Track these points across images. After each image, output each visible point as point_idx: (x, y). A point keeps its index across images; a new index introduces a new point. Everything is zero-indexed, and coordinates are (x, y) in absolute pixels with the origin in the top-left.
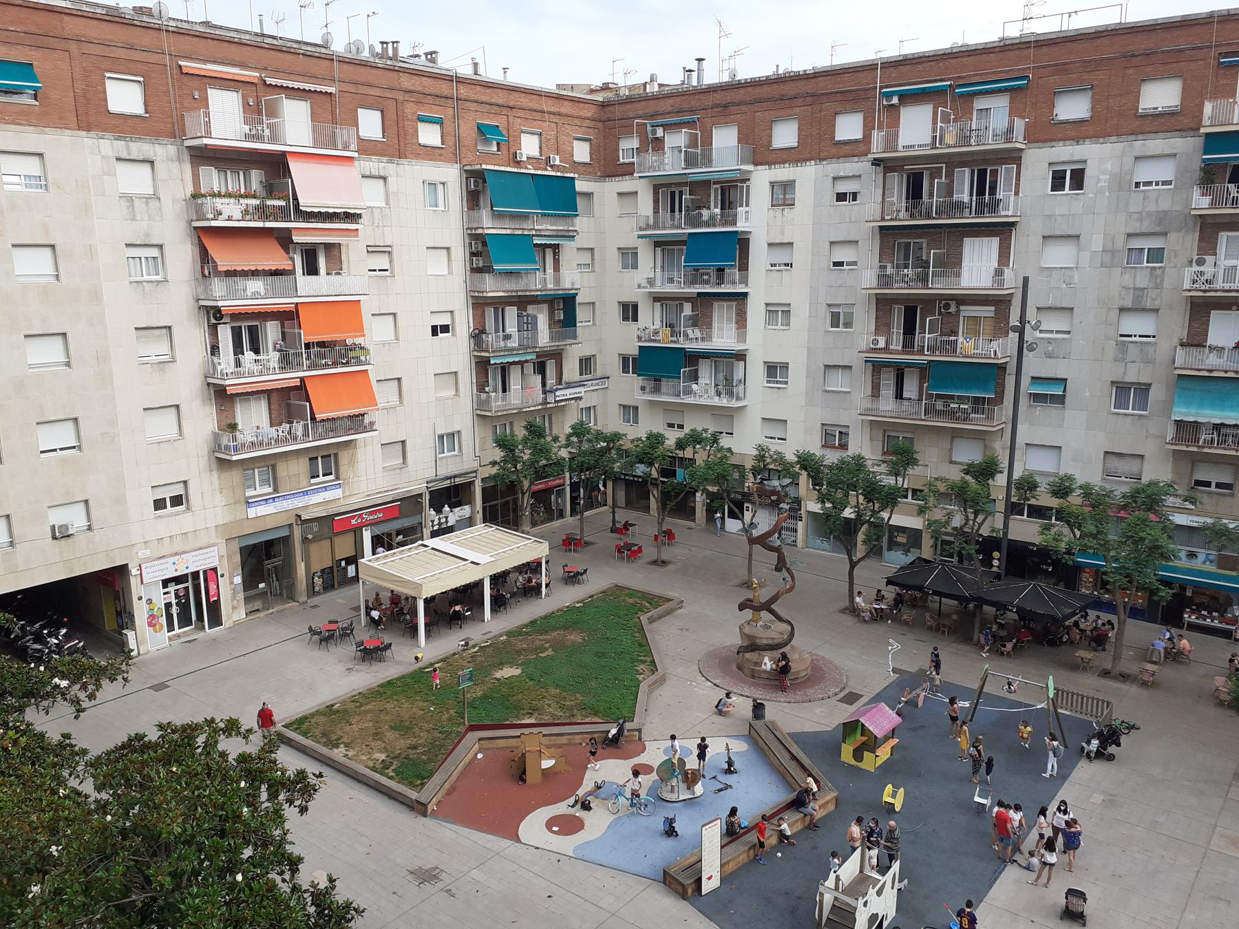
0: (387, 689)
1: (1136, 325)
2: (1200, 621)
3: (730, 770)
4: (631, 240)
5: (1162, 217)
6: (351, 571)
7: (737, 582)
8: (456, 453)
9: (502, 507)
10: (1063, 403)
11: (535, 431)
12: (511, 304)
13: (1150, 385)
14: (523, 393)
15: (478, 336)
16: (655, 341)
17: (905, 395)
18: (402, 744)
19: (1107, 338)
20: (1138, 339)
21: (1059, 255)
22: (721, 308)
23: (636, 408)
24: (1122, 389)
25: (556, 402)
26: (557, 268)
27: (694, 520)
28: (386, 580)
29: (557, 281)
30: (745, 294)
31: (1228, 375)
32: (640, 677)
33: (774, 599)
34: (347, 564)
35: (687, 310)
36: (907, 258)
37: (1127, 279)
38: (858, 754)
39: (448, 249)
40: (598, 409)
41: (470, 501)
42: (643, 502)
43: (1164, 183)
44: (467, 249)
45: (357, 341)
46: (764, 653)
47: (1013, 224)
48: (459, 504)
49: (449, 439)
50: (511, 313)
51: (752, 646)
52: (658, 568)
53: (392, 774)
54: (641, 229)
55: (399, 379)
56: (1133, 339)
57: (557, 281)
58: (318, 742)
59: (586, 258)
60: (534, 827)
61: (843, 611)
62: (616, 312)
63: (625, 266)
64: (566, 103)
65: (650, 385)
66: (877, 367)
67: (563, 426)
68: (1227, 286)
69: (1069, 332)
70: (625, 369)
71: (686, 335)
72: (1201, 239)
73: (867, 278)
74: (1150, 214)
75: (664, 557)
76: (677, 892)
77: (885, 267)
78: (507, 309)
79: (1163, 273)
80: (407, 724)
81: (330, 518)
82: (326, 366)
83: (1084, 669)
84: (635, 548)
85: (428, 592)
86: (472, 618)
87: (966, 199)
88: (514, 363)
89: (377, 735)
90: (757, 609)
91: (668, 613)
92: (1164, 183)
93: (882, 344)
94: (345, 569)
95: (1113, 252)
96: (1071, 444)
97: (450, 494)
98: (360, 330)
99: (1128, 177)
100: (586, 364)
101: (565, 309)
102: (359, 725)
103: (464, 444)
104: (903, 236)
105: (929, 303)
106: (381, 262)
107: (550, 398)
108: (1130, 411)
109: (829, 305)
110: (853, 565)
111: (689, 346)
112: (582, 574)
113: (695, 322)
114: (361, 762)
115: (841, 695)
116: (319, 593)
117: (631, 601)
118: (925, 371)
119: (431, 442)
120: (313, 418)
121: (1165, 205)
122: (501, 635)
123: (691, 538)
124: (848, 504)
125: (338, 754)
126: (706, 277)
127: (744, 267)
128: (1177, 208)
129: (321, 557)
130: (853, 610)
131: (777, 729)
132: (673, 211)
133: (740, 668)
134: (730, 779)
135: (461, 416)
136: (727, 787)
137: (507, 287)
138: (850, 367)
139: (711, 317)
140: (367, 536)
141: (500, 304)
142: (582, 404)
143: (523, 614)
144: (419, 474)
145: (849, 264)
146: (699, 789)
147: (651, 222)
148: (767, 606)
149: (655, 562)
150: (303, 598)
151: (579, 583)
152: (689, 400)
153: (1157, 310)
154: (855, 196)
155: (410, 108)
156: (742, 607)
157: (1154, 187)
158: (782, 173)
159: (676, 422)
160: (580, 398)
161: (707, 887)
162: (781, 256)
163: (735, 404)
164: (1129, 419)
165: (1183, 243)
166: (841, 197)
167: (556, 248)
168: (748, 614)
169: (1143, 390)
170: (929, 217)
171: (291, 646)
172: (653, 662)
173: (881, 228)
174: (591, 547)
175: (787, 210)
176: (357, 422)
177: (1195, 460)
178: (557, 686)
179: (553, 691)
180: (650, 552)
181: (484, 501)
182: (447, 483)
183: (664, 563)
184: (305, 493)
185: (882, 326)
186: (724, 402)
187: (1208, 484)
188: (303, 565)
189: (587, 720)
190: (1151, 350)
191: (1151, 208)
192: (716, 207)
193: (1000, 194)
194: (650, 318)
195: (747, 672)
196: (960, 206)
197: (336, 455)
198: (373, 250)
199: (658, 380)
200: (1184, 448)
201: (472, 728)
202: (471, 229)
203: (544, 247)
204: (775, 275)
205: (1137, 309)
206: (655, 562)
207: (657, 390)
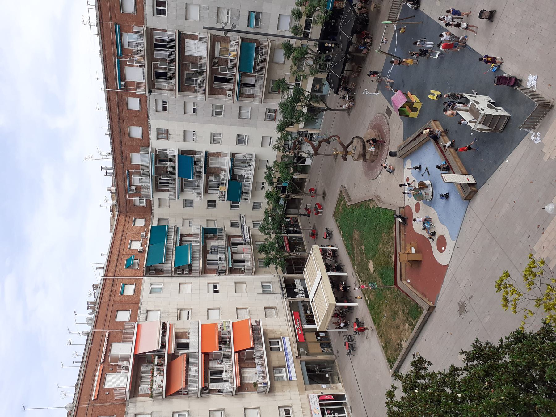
0: (376, 321)
4: (180, 202)
7: (334, 161)
8: (271, 285)
9: (296, 265)
12: (206, 257)
14: (245, 253)
15: (219, 272)
16: (225, 193)
23: (254, 203)
26: (191, 236)
27: (306, 179)
29: (196, 236)
30: (206, 152)
33: (342, 145)
35: (212, 178)
36: (193, 80)
38: (414, 110)
41: (293, 279)
42: (296, 201)
45: (219, 326)
46: (367, 150)
47: (180, 33)
49: (265, 288)
50: (210, 257)
51: (363, 155)
54: (175, 197)
55: (237, 309)
57: (196, 236)
58: (399, 354)
59: (187, 223)
61: (349, 114)
62: (211, 210)
63: (191, 205)
64: (118, 228)
65: (244, 196)
66: (241, 95)
67: (261, 236)
69: (228, 10)
71: (223, 179)
73: (201, 98)
75: (321, 193)
76: (474, 194)
77: (196, 90)
78: (208, 258)
81: (298, 343)
82: (230, 341)
83: (379, 7)
84: (317, 206)
85: (333, 301)
86: (346, 281)
87: (168, 53)
88: (232, 257)
89: (397, 327)
90: (347, 153)
91: (347, 193)
93: (230, 93)
94: (321, 337)
97: (289, 288)
98: (215, 325)
100: (234, 224)
101: (209, 233)
102: (392, 335)
103: (267, 281)
104: (183, 82)
105: (213, 71)
106: (184, 314)
107: (248, 241)
109: (212, 115)
110: (328, 109)
111: (228, 178)
113: (217, 175)
114: (409, 335)
115: (387, 116)
116: (332, 350)
118: (243, 74)
119: (266, 296)
120: (253, 348)
122: (354, 268)
123: (313, 180)
124: (299, 110)
125: (405, 345)
126: (198, 170)
127: (194, 153)
129: (315, 348)
130: (349, 109)
131: (401, 146)
132: (168, 183)
133: (373, 161)
134: (424, 168)
135: (255, 282)
136: (427, 169)
137: (198, 258)
138: (240, 107)
140: (307, 327)
141: (206, 262)
142: (251, 227)
143: (344, 258)
144: (280, 302)
145: (194, 106)
147: (172, 193)
148: (346, 148)
149: (324, 198)
150: (334, 357)
151: (332, 232)
152: (252, 179)
154: (164, 102)
155: (117, 298)
156: (345, 159)
158: (153, 134)
159: (261, 185)
160: (249, 228)
161: (472, 181)
162: (190, 136)
163: (254, 159)
166: (165, 108)
168: (348, 157)
170: (175, 70)
171: (355, 363)
172: (369, 200)
173: (179, 91)
174: (316, 227)
175: (170, 133)
176: (255, 329)
178: (378, 244)
179: (380, 246)
180: (319, 200)
182: (284, 289)
184: (286, 354)
185: (222, 92)
186: (253, 163)
188: (318, 356)
189: (394, 231)
194: (215, 195)
196: (171, 56)
198: (179, 318)
199: (242, 193)
201: (396, 284)
203: (181, 241)
206: (324, 198)
207: (247, 193)
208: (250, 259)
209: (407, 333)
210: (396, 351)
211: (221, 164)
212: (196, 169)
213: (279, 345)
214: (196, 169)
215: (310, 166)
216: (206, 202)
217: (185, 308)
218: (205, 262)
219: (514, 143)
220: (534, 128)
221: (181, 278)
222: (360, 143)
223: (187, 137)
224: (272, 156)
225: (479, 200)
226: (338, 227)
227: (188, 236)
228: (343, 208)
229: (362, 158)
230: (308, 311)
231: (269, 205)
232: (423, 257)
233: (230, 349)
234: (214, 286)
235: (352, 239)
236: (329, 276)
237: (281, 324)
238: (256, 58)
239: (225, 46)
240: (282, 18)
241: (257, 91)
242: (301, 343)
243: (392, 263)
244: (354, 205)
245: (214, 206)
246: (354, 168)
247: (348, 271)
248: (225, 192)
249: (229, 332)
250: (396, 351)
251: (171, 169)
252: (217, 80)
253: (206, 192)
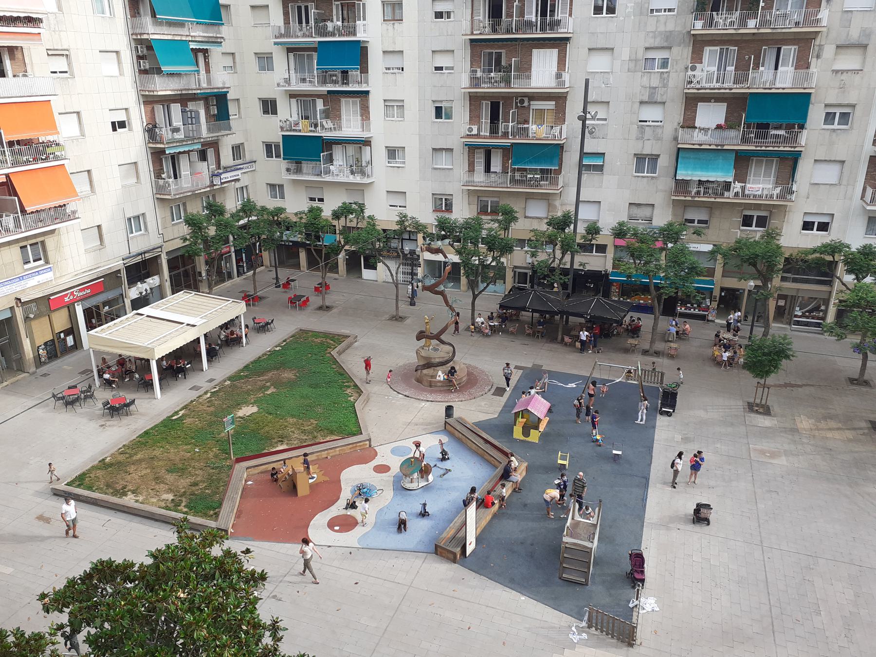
0: (146, 439)
1: (652, 114)
2: (687, 311)
3: (444, 457)
4: (267, 45)
5: (668, 35)
6: (70, 341)
7: (387, 317)
8: (143, 232)
9: (184, 274)
10: (602, 170)
11: (215, 210)
12: (175, 101)
13: (659, 156)
14: (193, 177)
15: (151, 131)
16: (295, 130)
18: (183, 483)
19: (632, 123)
20: (651, 124)
21: (599, 63)
22: (347, 103)
23: (281, 186)
24: (640, 159)
25: (222, 183)
26: (208, 71)
27: (337, 273)
28: (117, 347)
29: (209, 81)
30: (367, 92)
31: (703, 147)
32: (352, 399)
34: (66, 336)
35: (320, 105)
36: (490, 65)
37: (645, 81)
39: (117, 52)
41: (158, 272)
42: (292, 261)
43: (670, 10)
44: (134, 52)
45: (51, 138)
46: (438, 368)
47: (567, 39)
48: (148, 276)
49: (135, 222)
50: (176, 108)
51: (429, 365)
52: (325, 312)
53: (185, 510)
54: (276, 37)
55: (89, 171)
56: (648, 123)
57: (209, 81)
58: (106, 494)
59: (229, 61)
60: (318, 528)
62: (258, 108)
63: (262, 68)
65: (293, 166)
66: (472, 149)
67: (231, 204)
68: (707, 86)
69: (605, 120)
70: (269, 154)
71: (322, 126)
72: (693, 52)
73: (463, 80)
74: (661, 33)
76: (448, 558)
77: (476, 71)
78: (173, 106)
79: (668, 76)
80: (180, 466)
81: (47, 298)
82: (27, 162)
84: (305, 299)
85: (158, 355)
86: (193, 369)
87: (534, 20)
88: (184, 152)
89: (158, 479)
92: (670, 10)
93: (475, 132)
94: (65, 340)
95: (636, 60)
96: (610, 199)
97: (140, 269)
98: (53, 127)
99: (646, 5)
100: (237, 150)
101: (219, 105)
102: (135, 474)
103: (149, 224)
104: (488, 47)
105: (508, 98)
106: (60, 64)
107: (217, 181)
108: (645, 174)
109: (434, 101)
111: (325, 134)
112: (270, 324)
113: (327, 114)
114: (153, 504)
116: (45, 363)
118: (507, 151)
119: (122, 225)
120: (23, 211)
121: (670, 27)
122: (225, 381)
124: (467, 251)
125: (129, 500)
126: (334, 78)
127: (364, 70)
128: (678, 29)
129: (42, 332)
130: (478, 330)
131: (466, 422)
132: (300, 22)
134: (447, 465)
135: (144, 201)
136: (448, 471)
137: (177, 86)
138: (451, 150)
139: (339, 110)
140: (79, 310)
141: (166, 101)
142: (238, 185)
143: (234, 362)
144: (116, 255)
145: (447, 68)
146: (431, 477)
147: (283, 32)
149: (320, 308)
150: (33, 369)
151: (268, 330)
152: (328, 178)
153: (664, 103)
154: (449, 14)
156: (419, 338)
157: (663, 13)
159: (317, 197)
160: (238, 180)
161: (470, 549)
162: (394, 61)
163: (366, 180)
164: (645, 179)
165: (682, 54)
166: (439, 15)
167: (205, 52)
169: (654, 158)
170: (509, 31)
171: (39, 412)
172: (356, 386)
173: (472, 41)
174: (264, 301)
175: (397, 24)
176: (60, 213)
177: (686, 205)
178: (293, 416)
180: (315, 300)
181: (171, 269)
182: (139, 259)
183: (328, 308)
184: (21, 278)
185: (474, 117)
186: (358, 179)
187: (692, 221)
188: (28, 340)
189: (328, 439)
190: (659, 131)
191: (662, 28)
192: (338, 20)
193: (559, 16)
194: (288, 112)
196: (529, 25)
197: (43, 243)
198: (52, 53)
199: (299, 163)
200: (683, 198)
201: (238, 460)
202: (136, 34)
203: (195, 51)
204: (390, 77)
205: (650, 102)
206: (320, 308)
207: (299, 171)
208: (181, 188)
209: (154, 500)
210: (108, 486)
211: (349, 120)
212: (335, 75)
213: (34, 261)
214: (335, 75)
215: (360, 277)
216: (272, 96)
217: (74, 64)
218: (166, 101)
219: (555, 603)
220: (589, 627)
221: (128, 53)
222: (447, 357)
223: (391, 56)
225: (443, 569)
226: (284, 341)
227: (207, 64)
228: (322, 343)
229: (421, 363)
230: (107, 308)
231: (296, 214)
232: (305, 497)
233: (15, 164)
234: (124, 122)
235: (278, 369)
236: (198, 339)
237: (76, 259)
238: (534, 171)
239: (549, 118)
241: (479, 176)
242: (46, 304)
244: (335, 362)
245: (266, 112)
247: (211, 370)
248: (300, 131)
249: (46, 160)
250: (108, 486)
251: (330, 29)
252: (495, 108)
253: (292, 95)
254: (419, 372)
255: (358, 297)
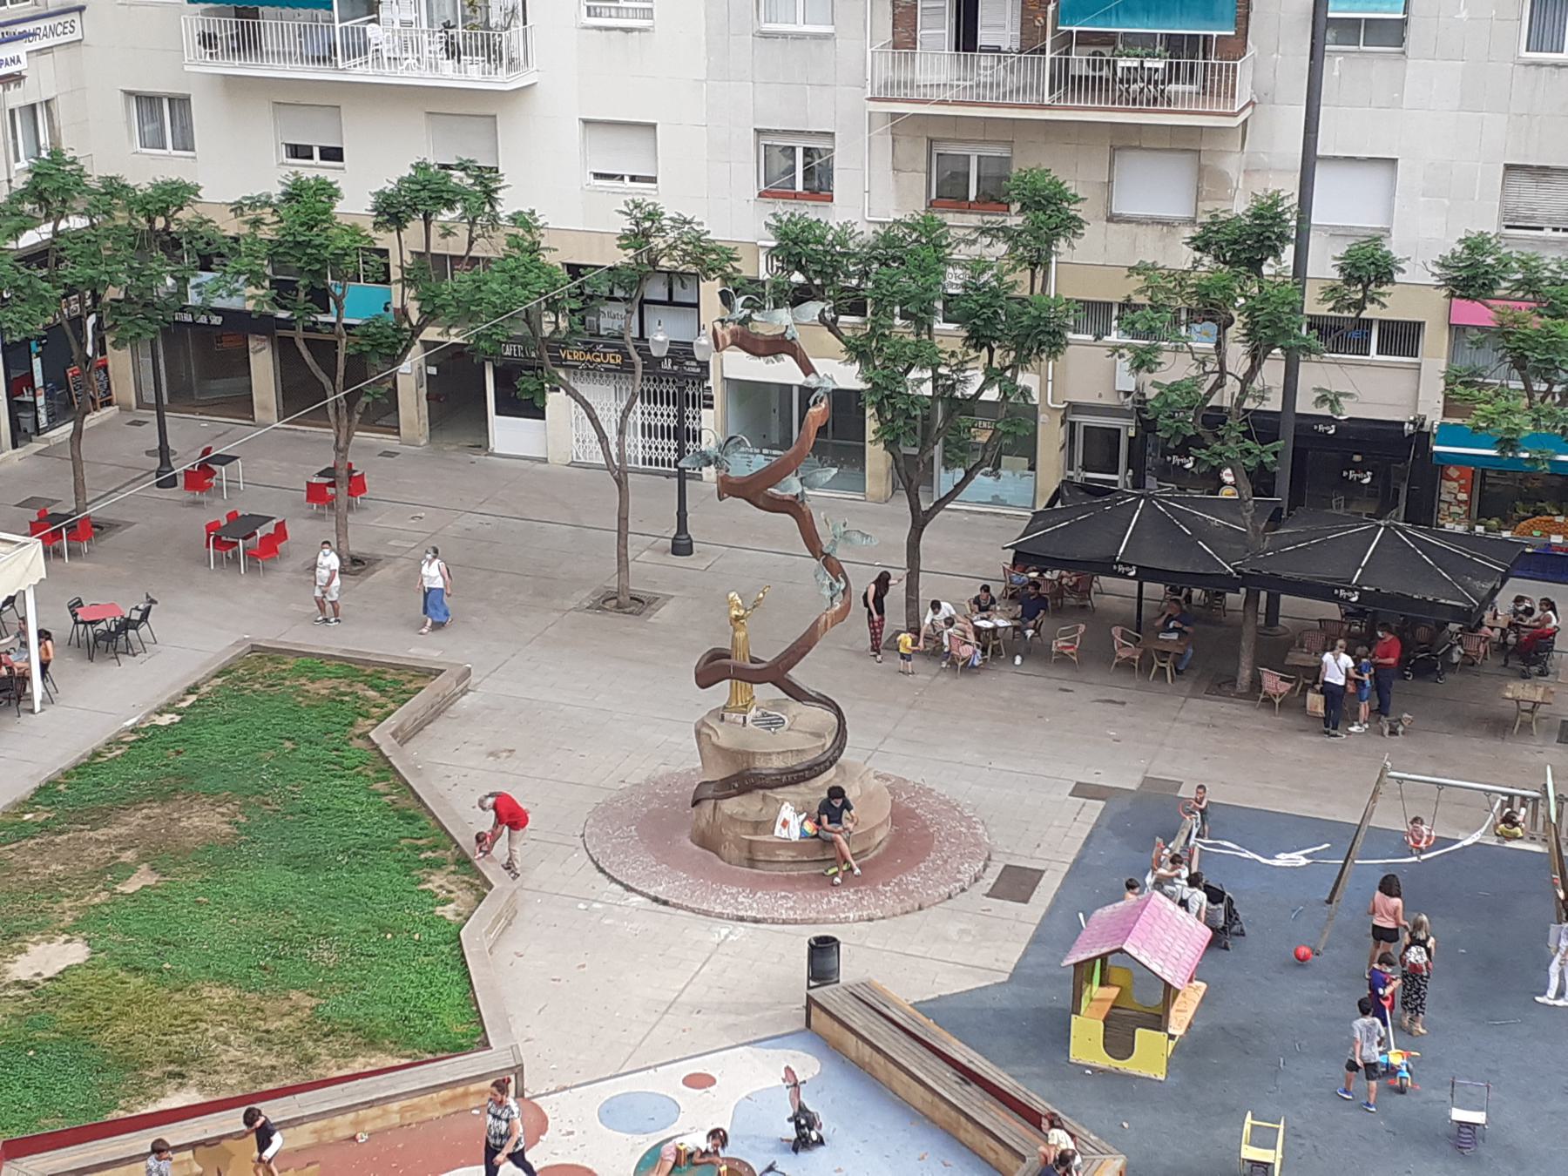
7: (585, 596)
10: (1400, 41)
17: (984, 38)
23: (180, 103)
27: (395, 429)
32: (448, 912)
38: (1118, 1039)
40: (60, 109)
46: (779, 793)
51: (745, 780)
83: (1526, 727)
84: (269, 528)
91: (437, 711)
115: (990, 879)
117: (322, 688)
124: (892, 348)
148: (777, 674)
151: (129, 650)
156: (705, 678)
159: (317, 141)
163: (503, 80)
168: (722, 691)
174: (110, 541)
178: (223, 979)
179: (217, 995)
186: (472, 74)
189: (357, 1066)
195: (731, 851)
199: (246, 13)
207: (247, 43)
215: (483, 445)
222: (814, 750)
224: (566, 203)
228: (336, 699)
229: (718, 773)
235: (165, 798)
238: (1134, 43)
240: (1374, 179)
241: (936, 62)
243: (141, 1092)
244: (387, 769)
246: (645, 725)
254: (708, 806)
255: (472, 521)
